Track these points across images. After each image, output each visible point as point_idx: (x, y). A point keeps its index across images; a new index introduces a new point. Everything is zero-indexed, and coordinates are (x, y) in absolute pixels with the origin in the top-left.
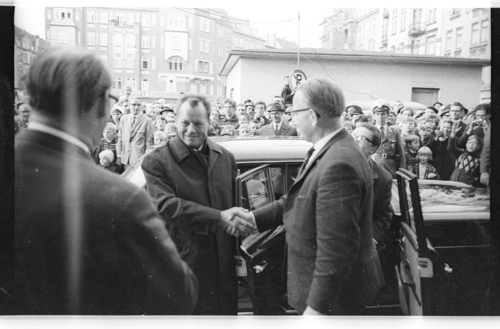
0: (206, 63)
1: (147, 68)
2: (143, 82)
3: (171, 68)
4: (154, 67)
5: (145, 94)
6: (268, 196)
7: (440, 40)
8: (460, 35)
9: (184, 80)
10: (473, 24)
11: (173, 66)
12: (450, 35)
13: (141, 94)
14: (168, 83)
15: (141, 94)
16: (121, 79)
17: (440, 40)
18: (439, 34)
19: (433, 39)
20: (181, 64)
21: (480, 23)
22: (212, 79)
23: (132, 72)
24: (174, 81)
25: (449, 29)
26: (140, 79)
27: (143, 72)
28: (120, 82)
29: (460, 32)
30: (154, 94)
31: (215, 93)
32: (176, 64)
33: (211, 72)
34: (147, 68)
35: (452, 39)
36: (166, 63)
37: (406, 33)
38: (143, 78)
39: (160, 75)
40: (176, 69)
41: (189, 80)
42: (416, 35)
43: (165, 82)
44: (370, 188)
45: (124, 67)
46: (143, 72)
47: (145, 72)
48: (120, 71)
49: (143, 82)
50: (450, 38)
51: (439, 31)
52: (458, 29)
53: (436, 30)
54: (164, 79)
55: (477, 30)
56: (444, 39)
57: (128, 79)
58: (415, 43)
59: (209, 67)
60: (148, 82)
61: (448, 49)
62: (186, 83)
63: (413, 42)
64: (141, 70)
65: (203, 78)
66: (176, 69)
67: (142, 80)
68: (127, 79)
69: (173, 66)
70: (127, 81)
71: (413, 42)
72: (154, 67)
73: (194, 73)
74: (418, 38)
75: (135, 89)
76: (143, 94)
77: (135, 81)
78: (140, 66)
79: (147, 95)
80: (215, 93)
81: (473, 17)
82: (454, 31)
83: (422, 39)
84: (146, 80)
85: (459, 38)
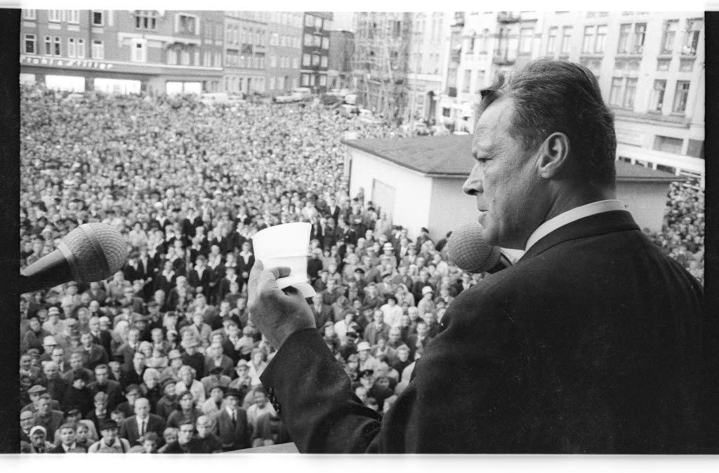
0: (190, 18)
1: (100, 23)
2: (94, 45)
3: (138, 26)
4: (111, 23)
5: (99, 64)
6: (463, 176)
7: (539, 36)
8: (569, 36)
9: (159, 45)
10: (586, 27)
11: (142, 22)
12: (554, 32)
13: (93, 65)
14: (134, 48)
15: (93, 65)
16: (60, 38)
17: (539, 36)
18: (539, 28)
19: (529, 32)
20: (154, 20)
21: (596, 27)
22: (198, 42)
23: (76, 29)
24: (143, 46)
25: (554, 25)
26: (90, 39)
27: (95, 30)
28: (57, 45)
29: (568, 32)
30: (113, 64)
31: (277, 81)
32: (146, 20)
33: (197, 32)
34: (100, 23)
35: (556, 39)
36: (132, 17)
37: (494, 18)
38: (93, 39)
39: (121, 35)
40: (146, 25)
41: (166, 44)
42: (506, 22)
43: (129, 47)
44: (551, 166)
45: (64, 20)
46: (95, 30)
47: (98, 30)
48: (58, 27)
49: (94, 45)
50: (555, 36)
51: (539, 24)
52: (565, 27)
53: (535, 21)
54: (127, 43)
55: (591, 35)
56: (545, 37)
57: (72, 40)
58: (504, 32)
59: (194, 25)
60: (101, 46)
61: (550, 50)
62: (162, 49)
63: (502, 30)
64: (91, 27)
65: (187, 41)
66: (146, 25)
67: (93, 41)
68: (69, 39)
69: (142, 22)
70: (69, 43)
71: (502, 30)
72: (111, 23)
73: (174, 35)
74: (509, 26)
75: (83, 57)
76: (96, 65)
77: (83, 44)
78: (90, 20)
79: (102, 67)
80: (277, 81)
81: (587, 17)
82: (560, 29)
83: (515, 29)
84: (99, 43)
85: (566, 39)
